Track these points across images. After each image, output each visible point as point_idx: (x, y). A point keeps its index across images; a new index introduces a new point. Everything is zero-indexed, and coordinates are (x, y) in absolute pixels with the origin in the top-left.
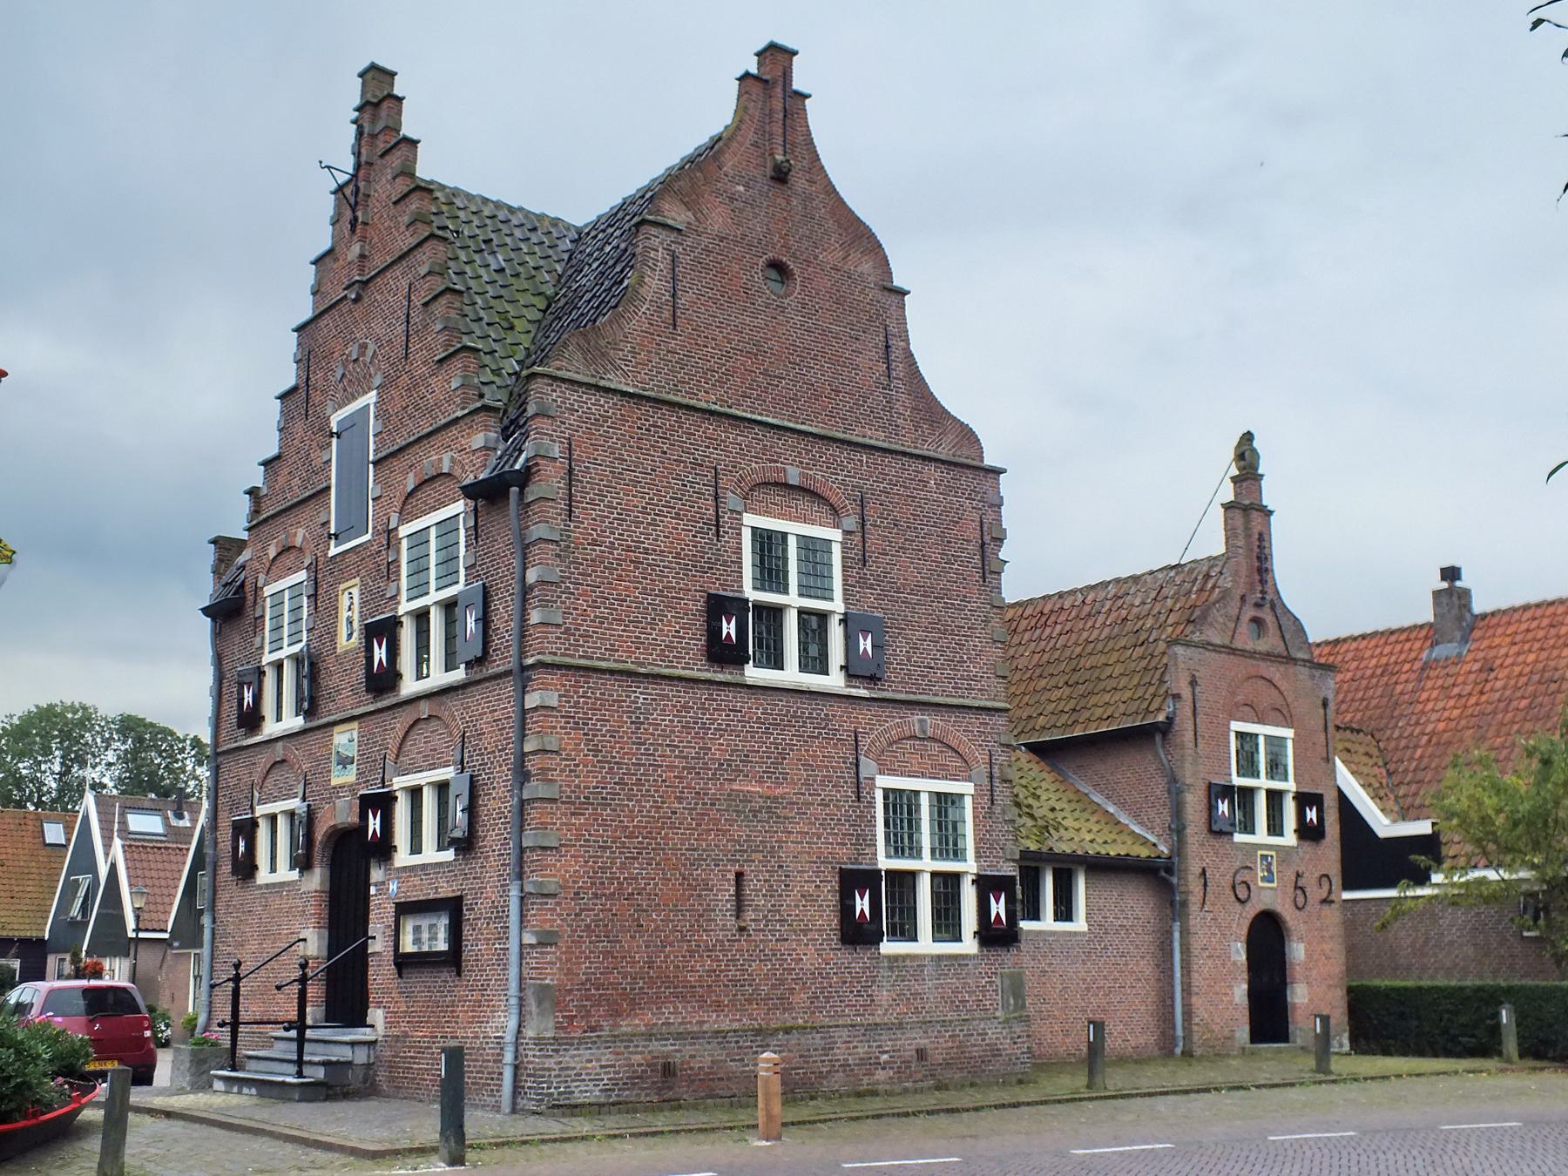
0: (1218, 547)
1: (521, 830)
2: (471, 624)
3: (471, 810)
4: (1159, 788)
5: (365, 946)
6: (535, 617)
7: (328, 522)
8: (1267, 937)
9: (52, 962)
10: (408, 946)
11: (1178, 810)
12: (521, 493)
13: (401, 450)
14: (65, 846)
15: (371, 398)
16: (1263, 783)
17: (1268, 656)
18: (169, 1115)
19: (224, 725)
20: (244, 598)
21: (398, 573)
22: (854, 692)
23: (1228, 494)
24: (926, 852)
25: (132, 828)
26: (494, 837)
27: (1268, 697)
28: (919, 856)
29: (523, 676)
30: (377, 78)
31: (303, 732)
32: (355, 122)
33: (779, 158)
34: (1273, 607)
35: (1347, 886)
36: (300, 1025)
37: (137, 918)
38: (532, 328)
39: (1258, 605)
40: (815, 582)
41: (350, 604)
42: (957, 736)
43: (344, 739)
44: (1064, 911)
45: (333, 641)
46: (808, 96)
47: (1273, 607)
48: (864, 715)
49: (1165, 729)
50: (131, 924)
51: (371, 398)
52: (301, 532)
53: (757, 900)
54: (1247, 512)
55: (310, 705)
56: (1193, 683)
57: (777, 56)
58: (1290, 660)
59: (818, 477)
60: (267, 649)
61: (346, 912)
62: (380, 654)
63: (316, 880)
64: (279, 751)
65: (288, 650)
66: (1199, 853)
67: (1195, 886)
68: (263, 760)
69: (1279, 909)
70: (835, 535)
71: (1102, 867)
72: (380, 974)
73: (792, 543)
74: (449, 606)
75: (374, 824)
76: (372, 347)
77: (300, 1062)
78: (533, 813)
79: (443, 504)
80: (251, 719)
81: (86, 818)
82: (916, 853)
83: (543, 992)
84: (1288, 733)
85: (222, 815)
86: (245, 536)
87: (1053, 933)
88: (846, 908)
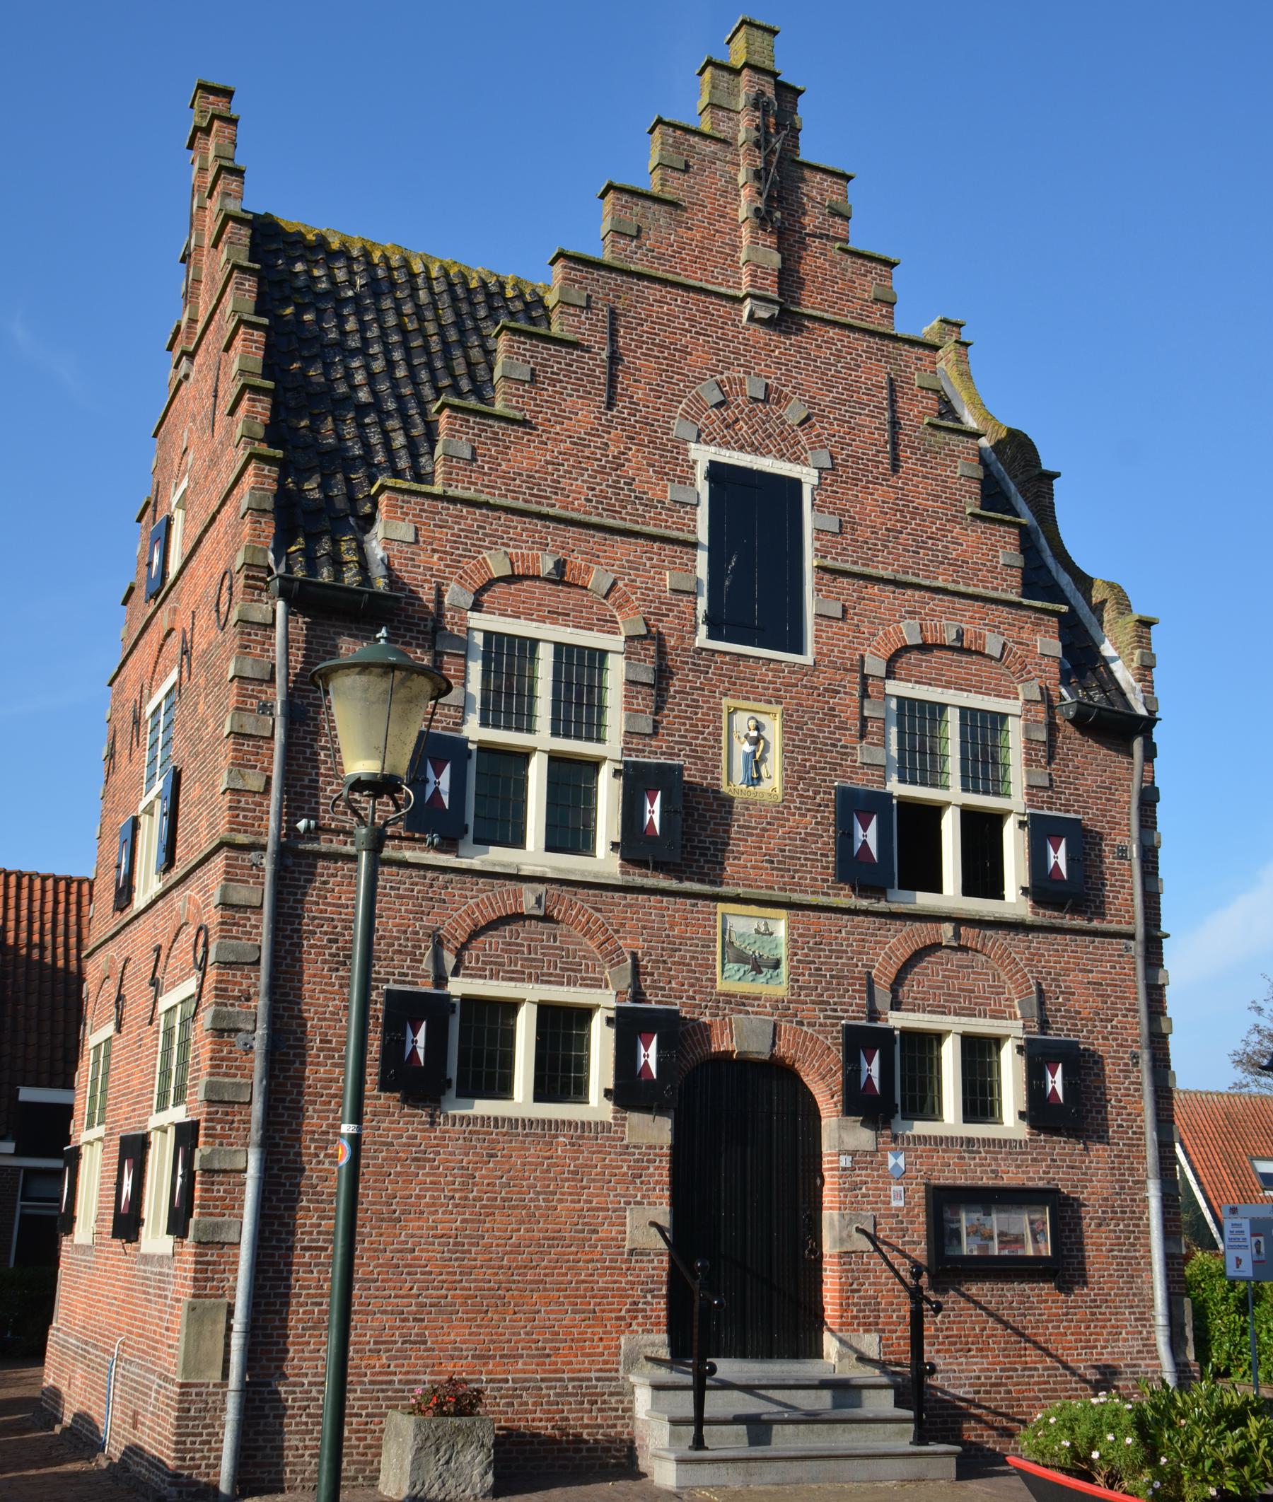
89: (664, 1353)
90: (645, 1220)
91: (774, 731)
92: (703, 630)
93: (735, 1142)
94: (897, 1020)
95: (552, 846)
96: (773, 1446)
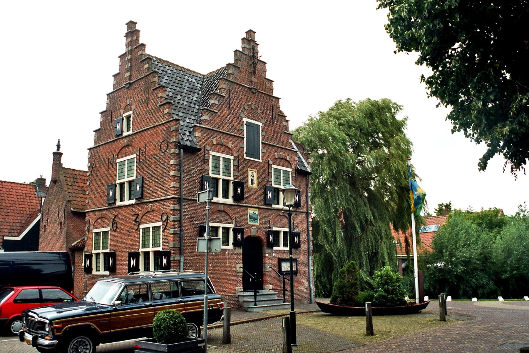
2: (138, 188)
16: (221, 176)
28: (149, 247)
30: (131, 24)
57: (250, 33)
74: (130, 183)
89: (242, 290)
90: (239, 267)
91: (255, 174)
92: (245, 155)
93: (253, 250)
94: (275, 229)
95: (223, 197)
96: (360, 92)
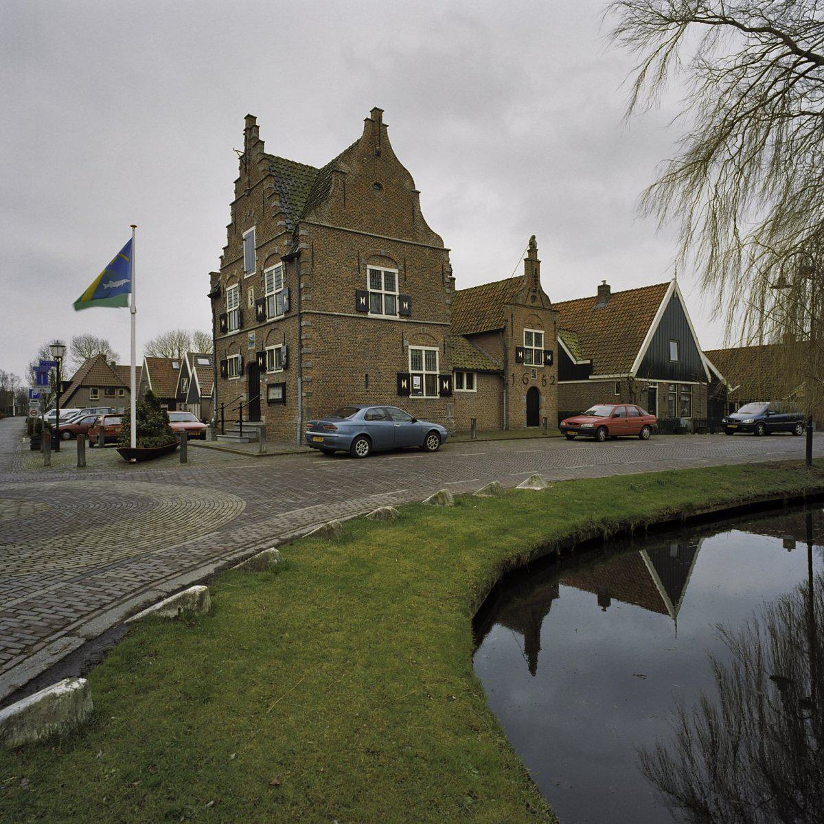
0: (523, 273)
1: (301, 362)
3: (287, 357)
4: (501, 349)
5: (259, 397)
6: (303, 298)
7: (243, 268)
8: (533, 394)
9: (178, 405)
10: (271, 397)
11: (506, 356)
12: (298, 260)
13: (263, 245)
14: (179, 370)
15: (254, 228)
17: (537, 308)
18: (207, 447)
19: (217, 332)
20: (220, 292)
21: (264, 284)
22: (402, 320)
23: (526, 256)
24: (424, 368)
25: (199, 363)
26: (294, 364)
27: (536, 321)
29: (300, 316)
30: (250, 119)
31: (239, 333)
32: (244, 134)
33: (378, 148)
34: (539, 292)
35: (559, 380)
36: (241, 421)
37: (201, 391)
38: (304, 205)
39: (534, 292)
40: (390, 286)
41: (251, 293)
42: (434, 334)
43: (251, 335)
44: (470, 386)
45: (247, 306)
46: (388, 126)
47: (539, 292)
48: (405, 327)
49: (503, 331)
50: (200, 394)
51: (254, 228)
52: (236, 271)
53: (372, 383)
54: (532, 263)
55: (241, 326)
56: (512, 316)
58: (544, 309)
59: (390, 253)
60: (228, 307)
61: (254, 388)
62: (260, 309)
63: (244, 379)
64: (233, 339)
65: (234, 308)
66: (514, 369)
67: (511, 380)
68: (229, 342)
69: (537, 386)
70: (396, 271)
71: (483, 373)
72: (264, 406)
73: (383, 274)
75: (261, 361)
76: (253, 211)
77: (241, 432)
78: (304, 358)
79: (276, 263)
80: (224, 330)
81: (185, 360)
82: (420, 368)
83: (309, 410)
84: (542, 332)
85: (218, 359)
86: (219, 272)
87: (467, 393)
88: (399, 385)
